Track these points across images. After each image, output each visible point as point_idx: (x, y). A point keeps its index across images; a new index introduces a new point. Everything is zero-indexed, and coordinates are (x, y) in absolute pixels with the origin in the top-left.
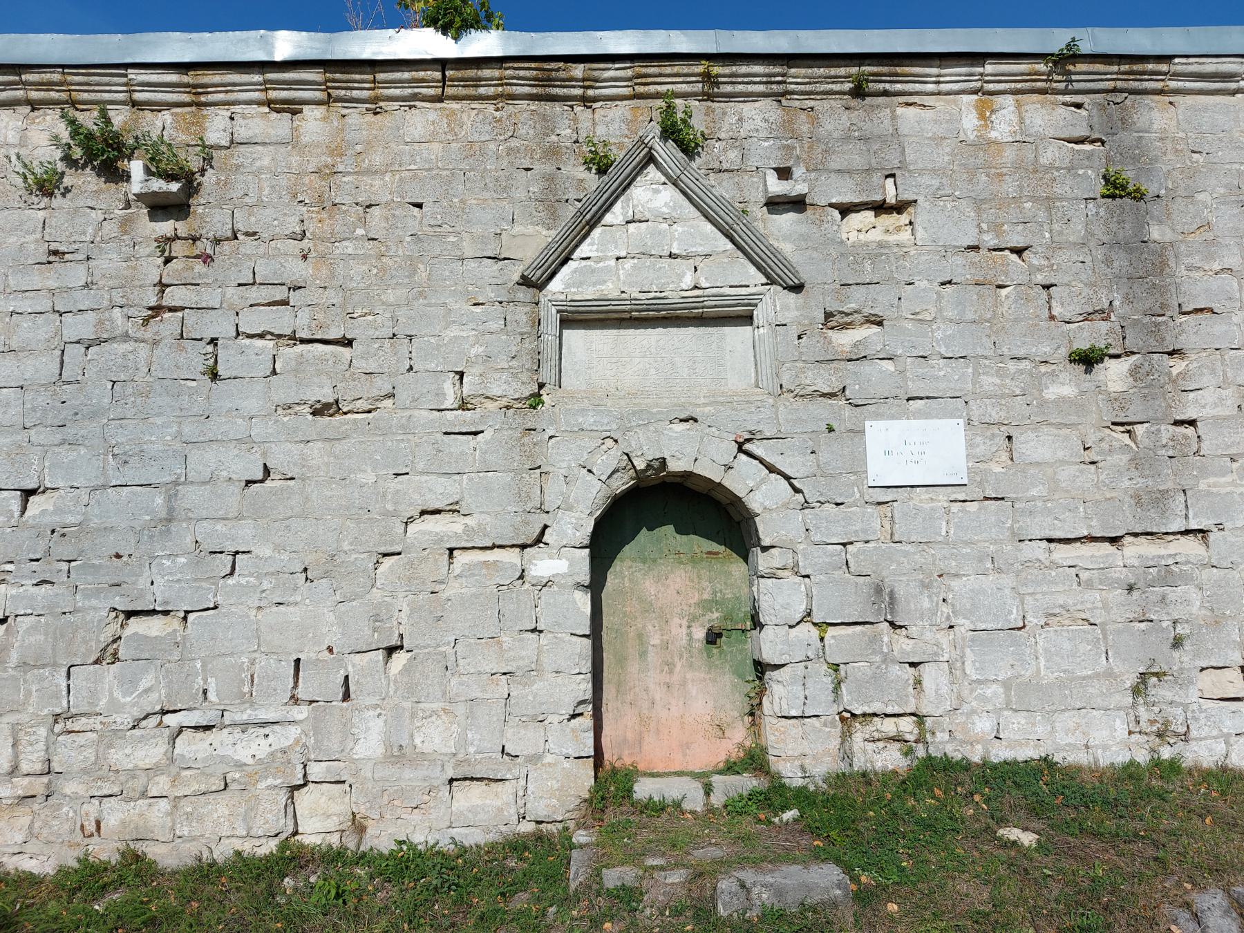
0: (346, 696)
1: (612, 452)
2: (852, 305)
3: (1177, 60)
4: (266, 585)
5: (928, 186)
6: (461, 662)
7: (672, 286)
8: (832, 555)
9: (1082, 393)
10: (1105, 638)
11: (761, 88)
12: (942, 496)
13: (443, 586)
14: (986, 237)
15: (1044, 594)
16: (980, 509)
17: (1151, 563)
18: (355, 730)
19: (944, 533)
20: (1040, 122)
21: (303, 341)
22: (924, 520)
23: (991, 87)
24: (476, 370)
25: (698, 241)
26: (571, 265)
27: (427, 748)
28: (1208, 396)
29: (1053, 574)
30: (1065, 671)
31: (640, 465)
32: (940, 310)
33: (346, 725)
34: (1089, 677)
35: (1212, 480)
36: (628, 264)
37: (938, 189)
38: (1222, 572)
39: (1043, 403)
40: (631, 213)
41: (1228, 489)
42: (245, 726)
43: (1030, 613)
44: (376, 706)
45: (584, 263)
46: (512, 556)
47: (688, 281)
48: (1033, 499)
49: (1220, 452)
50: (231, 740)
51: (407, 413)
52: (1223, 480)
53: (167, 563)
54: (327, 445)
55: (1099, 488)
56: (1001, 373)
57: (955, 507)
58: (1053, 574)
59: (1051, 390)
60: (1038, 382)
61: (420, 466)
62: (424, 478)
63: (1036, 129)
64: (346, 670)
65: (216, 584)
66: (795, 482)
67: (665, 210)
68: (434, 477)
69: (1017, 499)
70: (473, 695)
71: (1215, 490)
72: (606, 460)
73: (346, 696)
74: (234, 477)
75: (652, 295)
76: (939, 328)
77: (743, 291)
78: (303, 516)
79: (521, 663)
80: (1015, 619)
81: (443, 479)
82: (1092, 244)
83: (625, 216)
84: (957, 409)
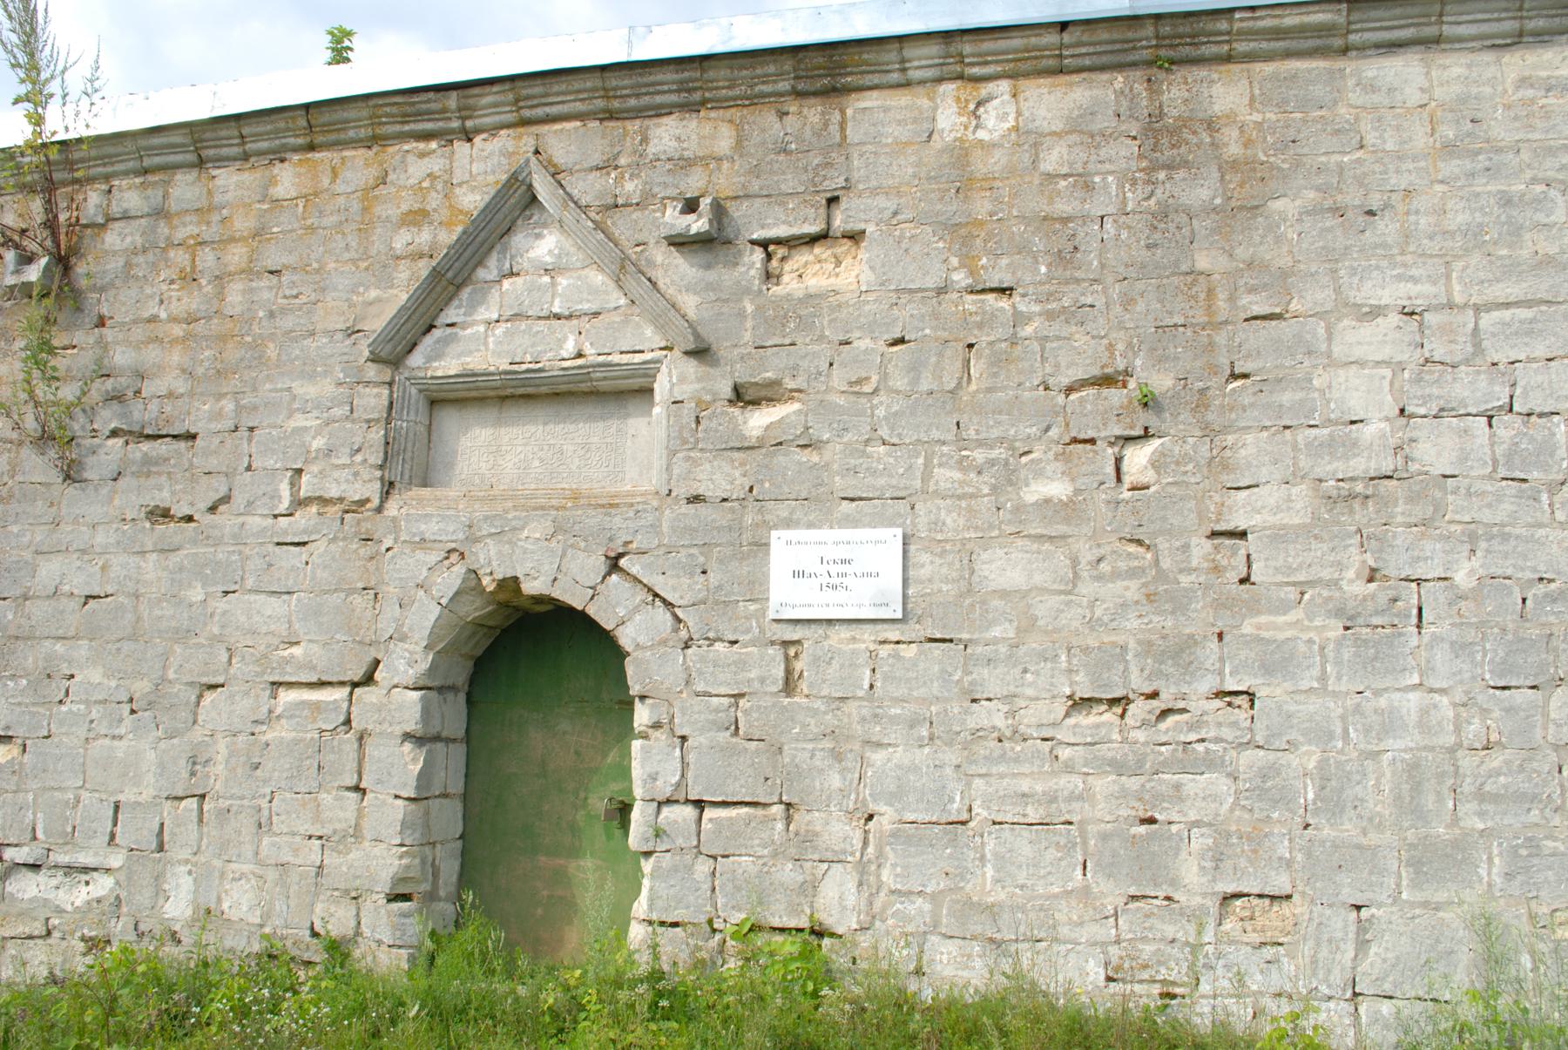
0: (161, 848)
1: (454, 569)
2: (769, 375)
3: (1237, 15)
4: (94, 715)
5: (881, 211)
6: (275, 818)
7: (550, 355)
8: (717, 711)
9: (1077, 491)
10: (1085, 843)
11: (674, 98)
12: (868, 635)
13: (264, 728)
14: (956, 277)
15: (1002, 776)
16: (921, 653)
17: (1164, 739)
18: (166, 887)
19: (866, 686)
20: (1042, 112)
21: (148, 437)
22: (842, 666)
23: (976, 70)
24: (315, 469)
25: (585, 296)
26: (436, 333)
27: (234, 915)
28: (1269, 495)
29: (1018, 748)
30: (1022, 887)
31: (488, 584)
32: (885, 377)
33: (159, 878)
34: (1056, 896)
35: (1263, 619)
36: (500, 330)
37: (895, 214)
38: (1272, 756)
39: (1018, 509)
40: (507, 265)
41: (1289, 634)
42: (70, 869)
43: (978, 802)
44: (187, 861)
45: (449, 330)
46: (341, 694)
47: (570, 347)
48: (996, 641)
49: (1280, 578)
50: (54, 882)
51: (241, 519)
52: (1281, 619)
53: (11, 684)
54: (162, 556)
55: (1092, 629)
56: (962, 464)
57: (884, 651)
58: (1018, 748)
59: (1033, 487)
60: (1009, 478)
61: (250, 583)
62: (253, 597)
63: (1037, 123)
64: (162, 817)
65: (50, 710)
66: (679, 612)
67: (548, 259)
68: (263, 596)
69: (970, 640)
70: (285, 859)
71: (1265, 634)
72: (450, 580)
73: (161, 848)
74: (76, 592)
75: (524, 367)
76: (881, 403)
77: (638, 358)
78: (133, 638)
79: (338, 826)
80: (956, 809)
81: (273, 599)
82: (1110, 279)
83: (500, 270)
84: (899, 514)
